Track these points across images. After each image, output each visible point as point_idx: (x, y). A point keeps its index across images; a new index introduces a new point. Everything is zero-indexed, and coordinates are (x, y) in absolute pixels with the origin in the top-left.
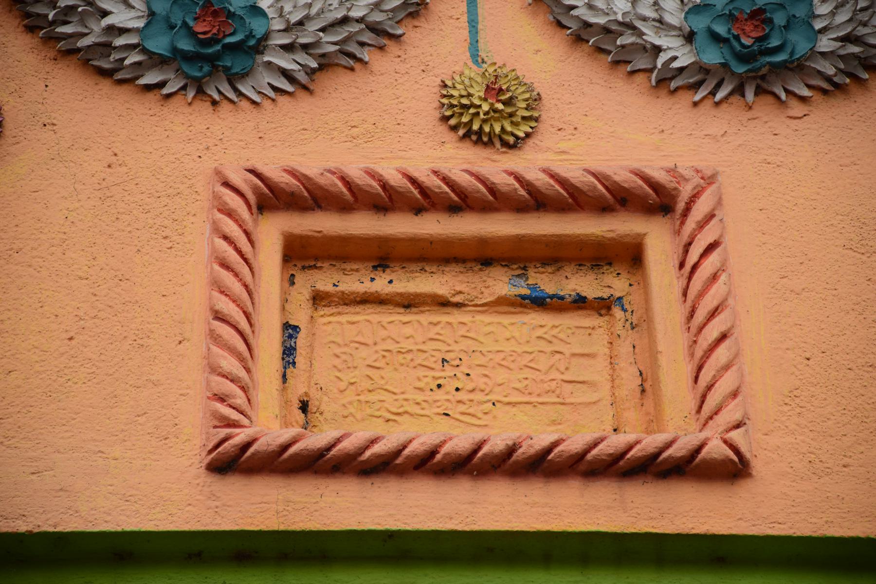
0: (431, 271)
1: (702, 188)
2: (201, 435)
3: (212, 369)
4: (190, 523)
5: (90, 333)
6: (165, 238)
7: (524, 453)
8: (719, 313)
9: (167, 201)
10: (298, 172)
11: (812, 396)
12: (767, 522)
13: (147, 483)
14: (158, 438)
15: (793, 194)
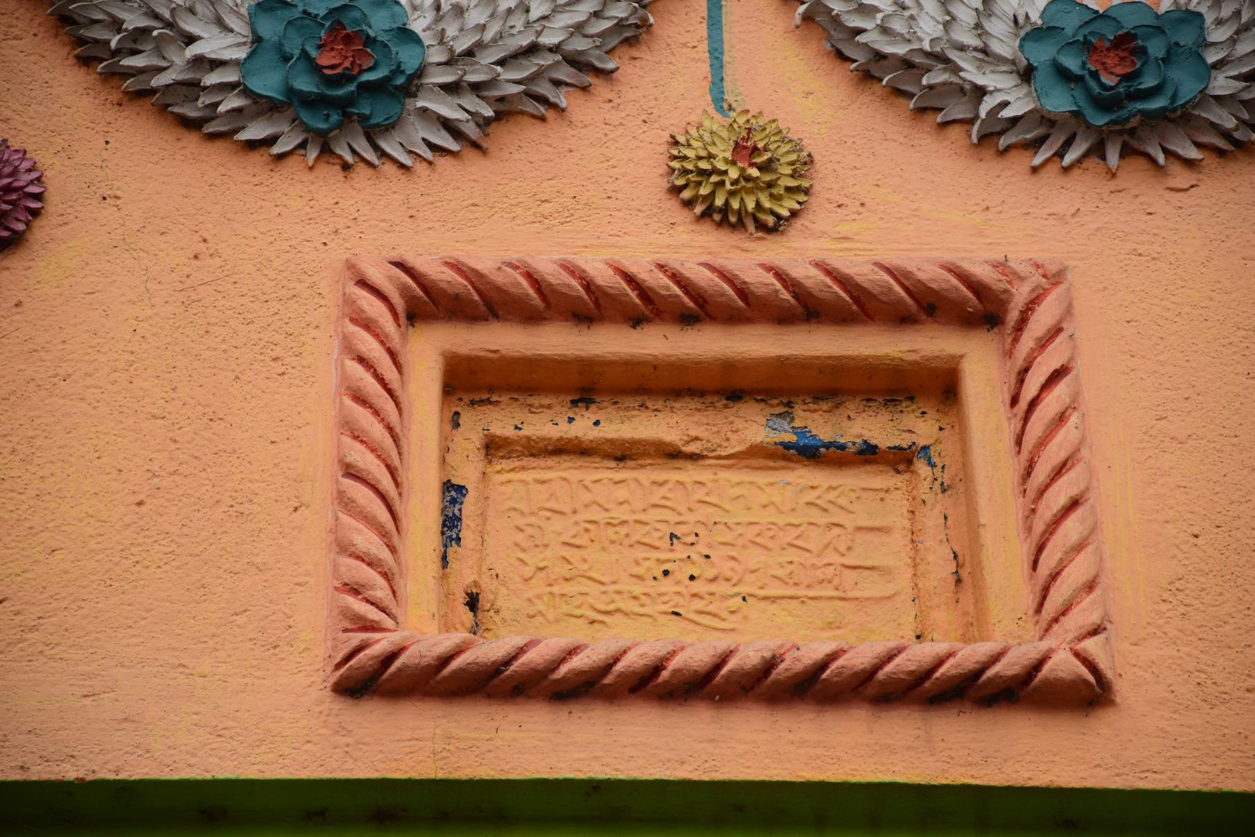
0: (655, 408)
1: (1044, 290)
2: (325, 642)
3: (341, 548)
4: (309, 768)
5: (168, 496)
6: (276, 359)
8: (1068, 470)
9: (278, 306)
10: (466, 265)
11: (1202, 590)
12: (1137, 770)
13: (249, 711)
14: (264, 646)
15: (1174, 299)
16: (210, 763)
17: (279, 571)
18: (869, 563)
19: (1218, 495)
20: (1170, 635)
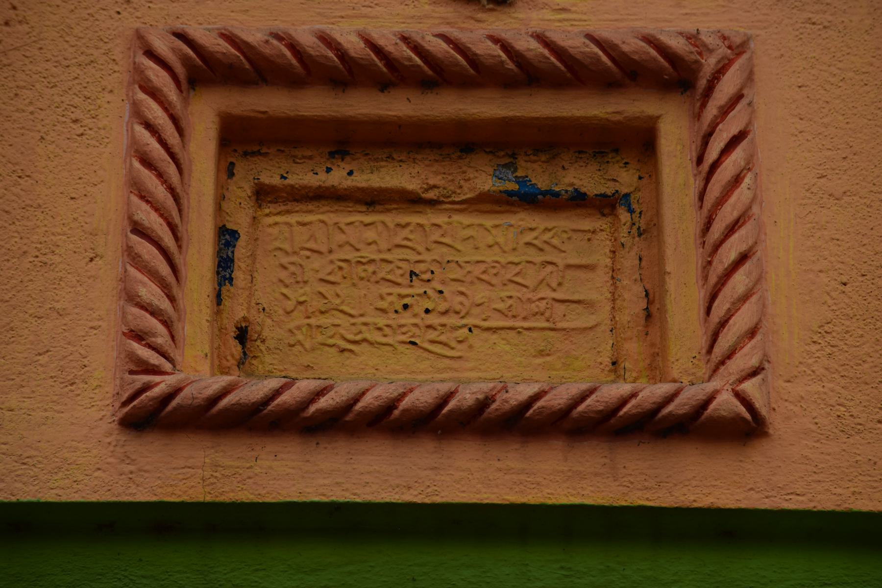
2: (114, 380)
3: (129, 297)
4: (99, 493)
6: (75, 121)
7: (497, 409)
8: (740, 227)
9: (78, 72)
10: (238, 38)
11: (847, 332)
13: (49, 442)
14: (63, 383)
15: (840, 65)
16: (16, 488)
17: (76, 316)
18: (576, 297)
19: (865, 247)
20: (818, 373)
